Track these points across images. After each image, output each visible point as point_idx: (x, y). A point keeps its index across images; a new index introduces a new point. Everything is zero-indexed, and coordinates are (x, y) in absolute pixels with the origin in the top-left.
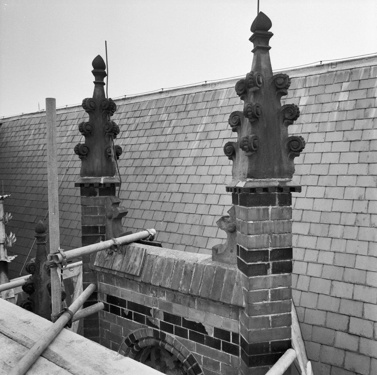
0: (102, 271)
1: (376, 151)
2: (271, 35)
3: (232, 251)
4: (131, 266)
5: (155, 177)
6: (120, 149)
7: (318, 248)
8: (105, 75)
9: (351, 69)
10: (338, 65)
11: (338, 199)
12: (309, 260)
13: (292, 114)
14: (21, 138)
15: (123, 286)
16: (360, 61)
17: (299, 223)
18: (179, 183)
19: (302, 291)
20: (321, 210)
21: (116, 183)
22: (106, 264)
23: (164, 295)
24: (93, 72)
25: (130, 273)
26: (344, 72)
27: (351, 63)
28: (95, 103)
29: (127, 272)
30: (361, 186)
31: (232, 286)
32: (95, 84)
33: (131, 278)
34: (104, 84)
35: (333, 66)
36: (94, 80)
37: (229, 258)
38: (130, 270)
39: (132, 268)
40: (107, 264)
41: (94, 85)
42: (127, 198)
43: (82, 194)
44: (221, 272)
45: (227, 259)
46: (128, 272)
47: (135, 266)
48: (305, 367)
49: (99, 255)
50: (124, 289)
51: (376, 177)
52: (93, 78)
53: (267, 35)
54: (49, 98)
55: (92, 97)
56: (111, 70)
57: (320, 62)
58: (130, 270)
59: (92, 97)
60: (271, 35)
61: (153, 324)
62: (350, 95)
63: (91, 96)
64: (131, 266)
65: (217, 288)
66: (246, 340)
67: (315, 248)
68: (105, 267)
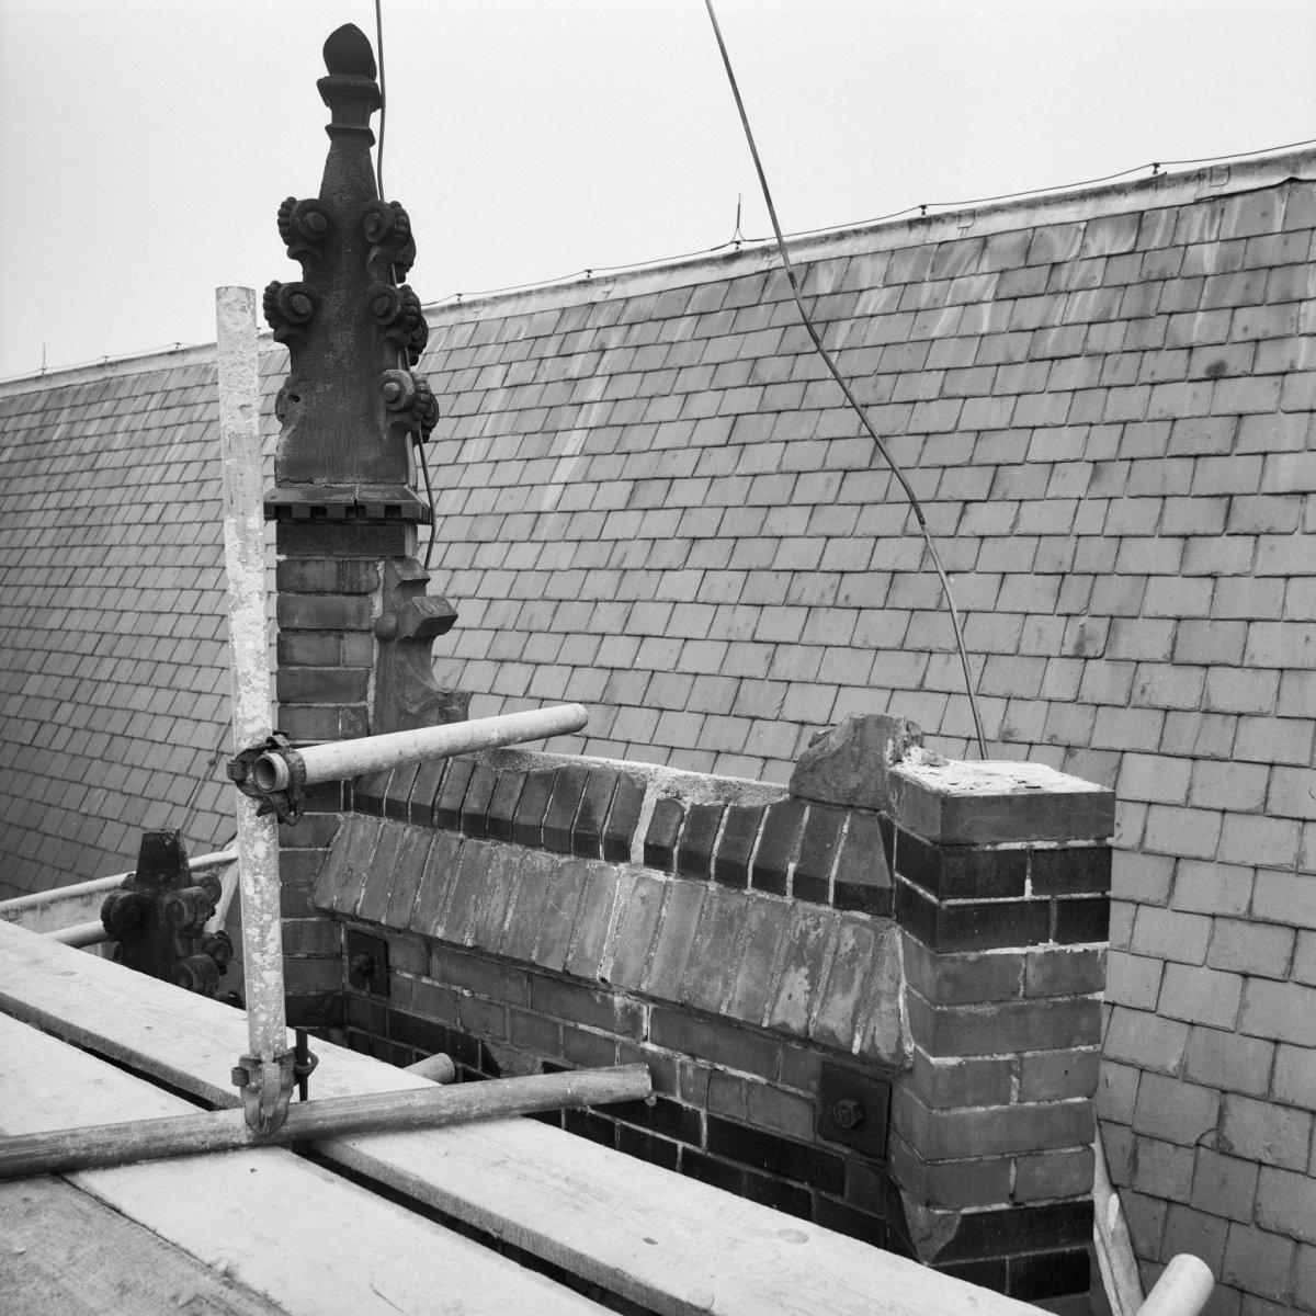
1: (1313, 622)
5: (500, 703)
8: (377, 100)
14: (188, 472)
18: (747, 472)
24: (323, 86)
28: (325, 214)
42: (1042, 496)
48: (1106, 1206)
51: (1310, 726)
55: (317, 197)
56: (395, 78)
57: (1153, 168)
59: (317, 197)
63: (314, 193)
66: (1035, 1246)
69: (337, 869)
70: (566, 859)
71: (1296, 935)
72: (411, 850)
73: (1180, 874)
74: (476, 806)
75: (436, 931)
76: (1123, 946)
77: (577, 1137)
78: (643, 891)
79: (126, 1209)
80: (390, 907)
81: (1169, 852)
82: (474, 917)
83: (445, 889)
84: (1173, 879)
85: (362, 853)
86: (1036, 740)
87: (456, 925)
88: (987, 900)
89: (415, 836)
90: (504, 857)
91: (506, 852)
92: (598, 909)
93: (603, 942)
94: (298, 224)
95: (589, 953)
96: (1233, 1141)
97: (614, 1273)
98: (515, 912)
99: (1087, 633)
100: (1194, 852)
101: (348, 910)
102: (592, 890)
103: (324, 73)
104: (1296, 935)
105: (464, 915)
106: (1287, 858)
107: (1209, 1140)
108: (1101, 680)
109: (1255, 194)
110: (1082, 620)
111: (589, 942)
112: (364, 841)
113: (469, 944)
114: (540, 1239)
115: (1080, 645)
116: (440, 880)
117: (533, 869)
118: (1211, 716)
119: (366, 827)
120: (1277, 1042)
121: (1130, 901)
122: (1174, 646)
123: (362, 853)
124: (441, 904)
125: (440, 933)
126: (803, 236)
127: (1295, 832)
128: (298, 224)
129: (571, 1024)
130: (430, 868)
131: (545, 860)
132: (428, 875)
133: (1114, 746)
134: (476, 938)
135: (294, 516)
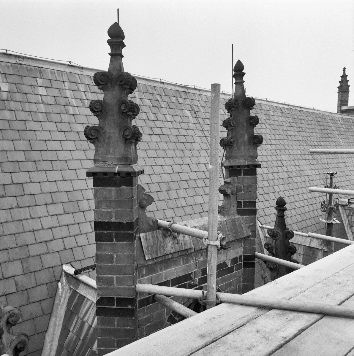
0: (155, 261)
2: (244, 74)
3: (233, 207)
4: (183, 243)
6: (256, 137)
7: (77, 222)
9: (38, 67)
10: (25, 59)
11: (74, 180)
12: (75, 234)
13: (96, 108)
15: (166, 268)
16: (43, 62)
17: (52, 205)
19: (80, 260)
20: (66, 191)
21: (108, 172)
22: (159, 252)
23: (202, 255)
24: (108, 42)
25: (185, 249)
26: (33, 68)
27: (36, 61)
29: (182, 250)
30: (86, 168)
31: (242, 227)
32: (110, 55)
33: (184, 253)
34: (235, 84)
35: (20, 59)
36: (110, 52)
37: (232, 211)
38: (183, 246)
39: (185, 244)
40: (160, 252)
41: (110, 57)
43: (95, 185)
44: (233, 221)
45: (231, 212)
46: (183, 249)
47: (186, 241)
49: (147, 248)
50: (169, 270)
52: (108, 49)
53: (242, 74)
54: (215, 84)
55: (247, 96)
58: (183, 246)
60: (244, 74)
61: (193, 284)
62: (47, 91)
64: (183, 243)
65: (236, 232)
67: (74, 223)
68: (159, 255)
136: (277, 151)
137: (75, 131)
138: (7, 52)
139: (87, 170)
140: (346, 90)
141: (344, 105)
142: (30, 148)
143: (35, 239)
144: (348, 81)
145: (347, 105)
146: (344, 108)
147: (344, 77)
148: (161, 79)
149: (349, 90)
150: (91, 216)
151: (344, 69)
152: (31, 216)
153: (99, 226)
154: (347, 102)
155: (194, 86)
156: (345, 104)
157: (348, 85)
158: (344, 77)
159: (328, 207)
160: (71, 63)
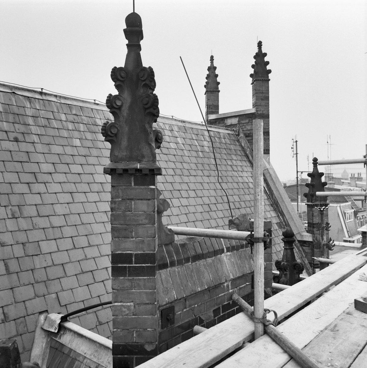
24: (124, 30)
55: (123, 66)
63: (123, 66)
69: (162, 290)
70: (213, 258)
71: (92, 273)
72: (181, 273)
73: (65, 268)
74: (193, 254)
75: (198, 290)
76: (61, 290)
77: (147, 362)
78: (228, 258)
79: (306, 344)
80: (184, 291)
81: (60, 263)
82: (204, 281)
83: (194, 278)
84: (64, 269)
85: (167, 282)
86: (13, 244)
87: (202, 285)
88: (140, 265)
89: (179, 269)
90: (202, 264)
91: (202, 262)
92: (224, 265)
93: (228, 271)
94: (116, 74)
95: (227, 275)
96: (102, 321)
97: (298, 305)
98: (211, 274)
99: (13, 211)
100: (66, 262)
101: (173, 300)
102: (220, 261)
103: (125, 27)
104: (92, 273)
105: (202, 282)
106: (84, 257)
107: (98, 324)
108: (23, 224)
109: (5, 93)
110: (10, 207)
111: (226, 273)
112: (166, 278)
113: (206, 288)
114: (227, 350)
115: (13, 215)
116: (192, 277)
117: (209, 263)
118: (54, 228)
119: (164, 274)
120: (99, 296)
121: (57, 279)
122: (38, 212)
123: (167, 282)
124: (195, 283)
125: (199, 289)
126: (82, 99)
127: (82, 251)
128: (116, 74)
129: (218, 296)
130: (188, 275)
131: (210, 260)
132: (189, 277)
133: (35, 240)
134: (207, 286)
135: (143, 173)
136: (204, 184)
137: (15, 161)
138: (95, 102)
139: (307, 173)
140: (216, 90)
141: (212, 113)
142: (34, 178)
143: (54, 280)
144: (217, 76)
145: (217, 112)
146: (212, 117)
147: (212, 69)
148: (95, 100)
149: (219, 89)
150: (107, 250)
151: (212, 58)
152: (58, 249)
153: (116, 258)
154: (217, 107)
155: (172, 116)
156: (214, 111)
157: (218, 81)
158: (212, 69)
159: (174, 337)
160: (96, 101)
